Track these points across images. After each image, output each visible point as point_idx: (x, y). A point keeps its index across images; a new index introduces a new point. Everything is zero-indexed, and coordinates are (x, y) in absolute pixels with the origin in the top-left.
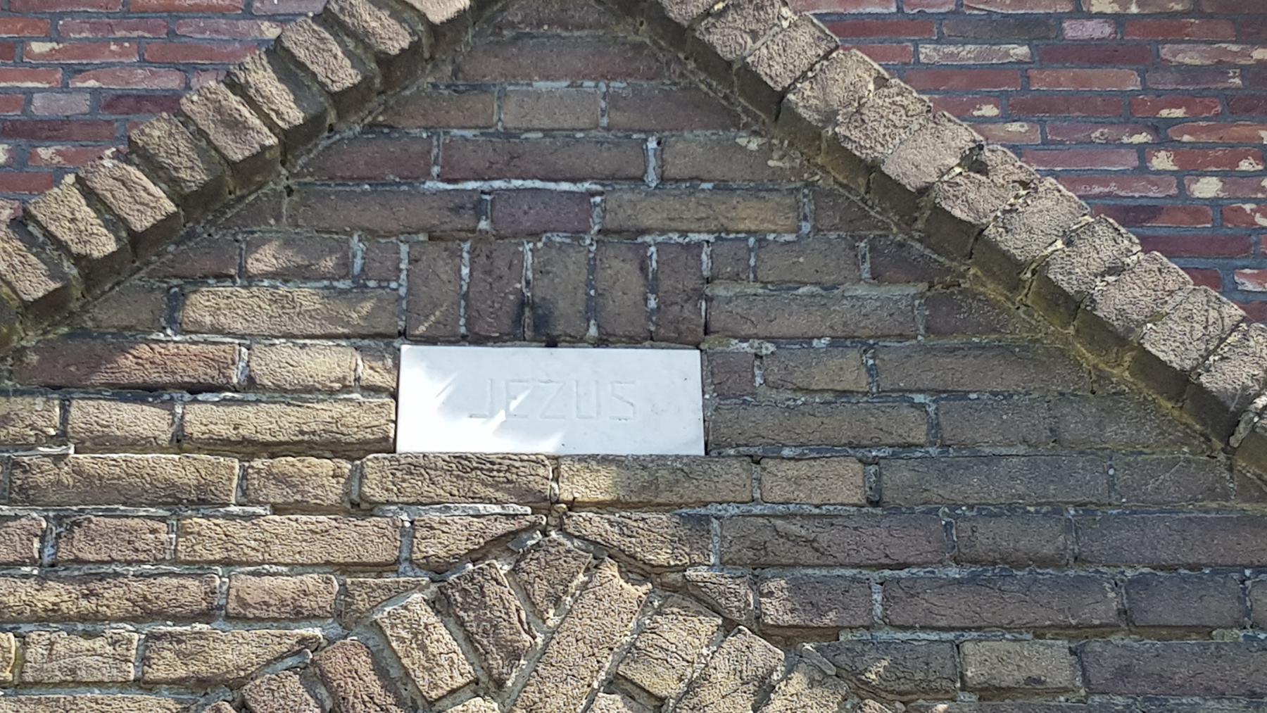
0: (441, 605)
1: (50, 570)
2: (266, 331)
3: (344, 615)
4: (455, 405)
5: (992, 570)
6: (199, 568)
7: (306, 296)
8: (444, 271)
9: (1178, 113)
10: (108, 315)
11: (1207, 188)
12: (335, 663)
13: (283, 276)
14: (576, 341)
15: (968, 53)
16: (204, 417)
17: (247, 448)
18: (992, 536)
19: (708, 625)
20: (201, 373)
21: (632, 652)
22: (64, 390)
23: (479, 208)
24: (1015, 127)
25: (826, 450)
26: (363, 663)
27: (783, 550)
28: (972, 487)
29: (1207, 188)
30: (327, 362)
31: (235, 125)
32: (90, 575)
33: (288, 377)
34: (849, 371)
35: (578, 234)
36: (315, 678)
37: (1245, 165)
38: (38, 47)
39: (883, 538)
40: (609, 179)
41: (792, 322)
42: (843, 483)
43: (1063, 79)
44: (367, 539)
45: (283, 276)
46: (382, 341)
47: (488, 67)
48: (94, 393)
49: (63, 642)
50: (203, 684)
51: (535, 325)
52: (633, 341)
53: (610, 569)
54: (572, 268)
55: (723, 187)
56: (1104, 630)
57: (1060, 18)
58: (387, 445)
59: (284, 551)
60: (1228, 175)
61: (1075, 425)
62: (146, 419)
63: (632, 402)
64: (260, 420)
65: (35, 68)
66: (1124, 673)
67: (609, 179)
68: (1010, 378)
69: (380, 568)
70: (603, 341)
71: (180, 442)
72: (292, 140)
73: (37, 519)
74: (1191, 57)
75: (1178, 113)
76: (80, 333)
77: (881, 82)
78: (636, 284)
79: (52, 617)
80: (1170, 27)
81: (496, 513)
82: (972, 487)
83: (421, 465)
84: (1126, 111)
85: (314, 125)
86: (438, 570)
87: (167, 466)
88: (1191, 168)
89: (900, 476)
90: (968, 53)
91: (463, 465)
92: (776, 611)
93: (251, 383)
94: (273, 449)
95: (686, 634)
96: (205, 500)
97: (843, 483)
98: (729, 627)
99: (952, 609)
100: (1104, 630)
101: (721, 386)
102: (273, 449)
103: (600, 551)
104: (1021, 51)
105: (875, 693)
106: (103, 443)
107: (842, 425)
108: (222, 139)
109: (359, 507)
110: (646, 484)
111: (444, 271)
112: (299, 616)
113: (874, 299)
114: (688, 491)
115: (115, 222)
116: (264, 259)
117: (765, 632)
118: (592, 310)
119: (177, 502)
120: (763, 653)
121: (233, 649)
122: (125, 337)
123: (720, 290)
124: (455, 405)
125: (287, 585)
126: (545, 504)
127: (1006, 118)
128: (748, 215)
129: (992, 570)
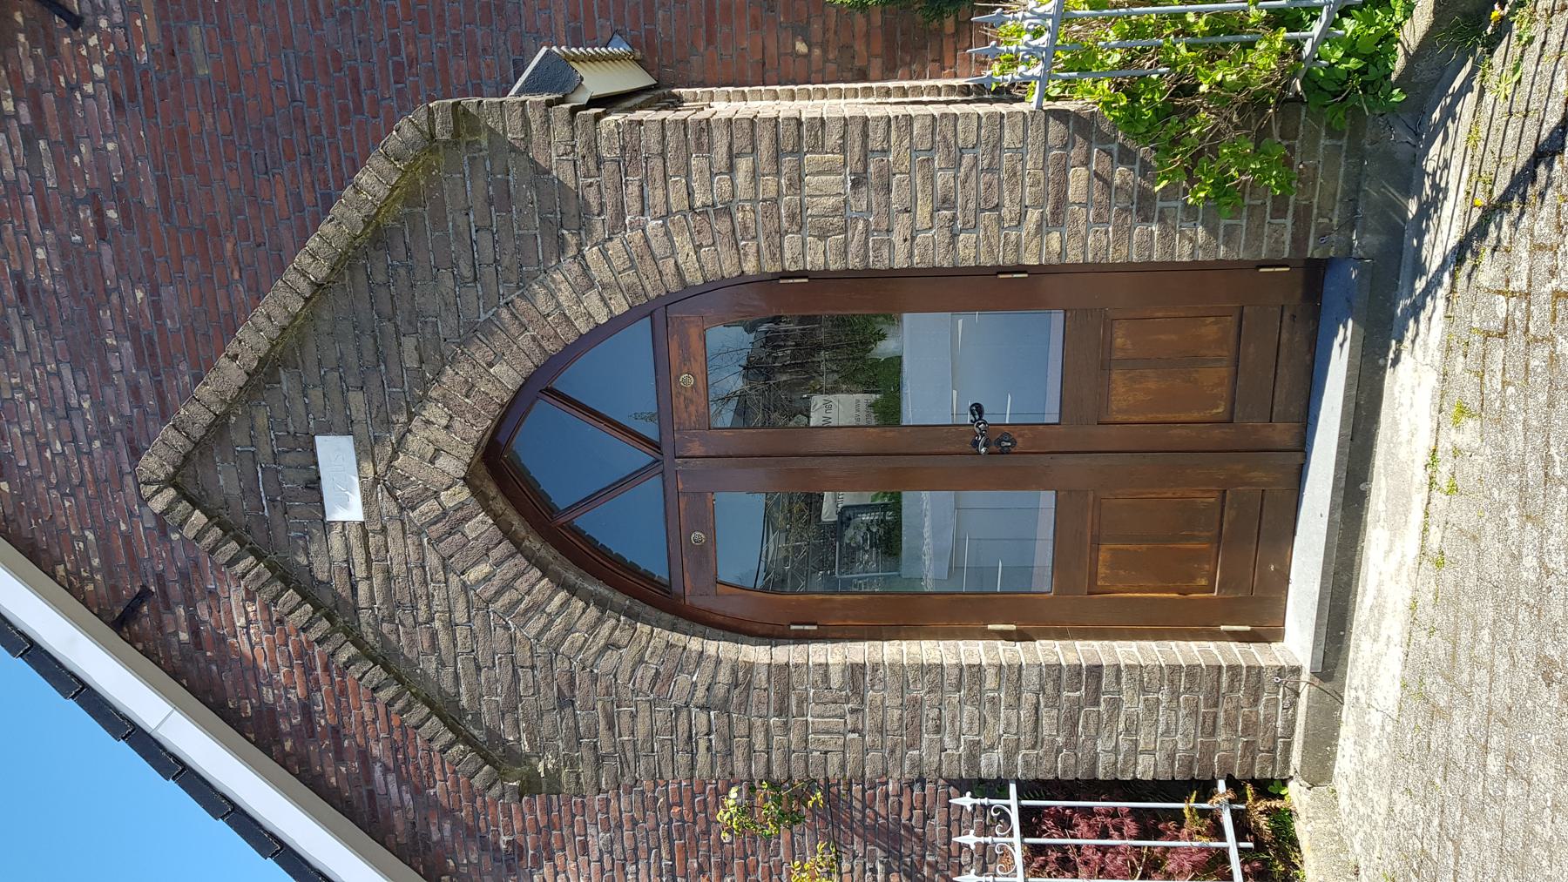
0: (413, 509)
1: (414, 607)
2: (326, 560)
3: (419, 533)
4: (345, 504)
5: (380, 357)
6: (409, 570)
7: (313, 548)
8: (298, 510)
9: (62, 79)
10: (329, 601)
11: (99, 70)
12: (434, 535)
13: (307, 555)
14: (318, 472)
15: (48, 167)
16: (360, 572)
17: (368, 561)
18: (369, 356)
19: (410, 437)
20: (345, 576)
21: (422, 457)
22: (356, 610)
23: (272, 500)
24: (83, 149)
25: (346, 402)
26: (434, 528)
27: (382, 415)
28: (352, 359)
29: (99, 70)
30: (336, 542)
31: (258, 575)
32: (414, 598)
33: (343, 551)
34: (316, 394)
35: (278, 472)
36: (440, 540)
37: (84, 53)
38: (123, 527)
39: (374, 382)
40: (255, 463)
41: (301, 409)
42: (356, 398)
43: (54, 127)
44: (394, 529)
45: (307, 555)
46: (327, 527)
47: (218, 500)
48: (356, 602)
49: (436, 602)
50: (444, 567)
51: (314, 484)
52: (315, 455)
53: (396, 463)
54: (291, 473)
55: (252, 428)
56: (396, 326)
57: (20, 125)
58: (362, 524)
59: (399, 550)
60: (90, 60)
61: (326, 328)
62: (363, 588)
63: (336, 456)
64: (358, 557)
65: (133, 527)
66: (410, 323)
67: (255, 463)
68: (311, 347)
69: (403, 523)
70: (316, 464)
71: (369, 578)
72: (260, 558)
73: (399, 612)
74: (30, 70)
75: (62, 79)
76: (336, 607)
77: (206, 384)
78: (293, 454)
79: (429, 606)
80: (15, 79)
81: (381, 494)
82: (352, 359)
83: (368, 514)
84: (65, 101)
85: (253, 552)
86: (402, 509)
87: (377, 580)
88: (91, 77)
89: (351, 380)
90: (48, 167)
91: (366, 503)
92: (403, 419)
93: (346, 561)
94: (368, 553)
95: (413, 442)
96: (388, 571)
97: (356, 398)
98: (409, 431)
99: (395, 370)
100: (396, 326)
101: (328, 430)
102: (368, 553)
103: (389, 466)
104: (42, 144)
105: (425, 392)
106: (372, 598)
107: (336, 396)
108: (264, 578)
109: (384, 530)
110: (364, 452)
111: (298, 510)
112: (421, 544)
113: (286, 381)
114: (366, 442)
115: (300, 605)
116: (303, 560)
117: (410, 420)
118: (306, 468)
119: (388, 576)
120: (416, 422)
121: (433, 560)
122: (336, 596)
123: (292, 429)
124: (345, 504)
125: (411, 548)
126: (376, 481)
127: (79, 153)
128: (262, 421)
129: (380, 357)
